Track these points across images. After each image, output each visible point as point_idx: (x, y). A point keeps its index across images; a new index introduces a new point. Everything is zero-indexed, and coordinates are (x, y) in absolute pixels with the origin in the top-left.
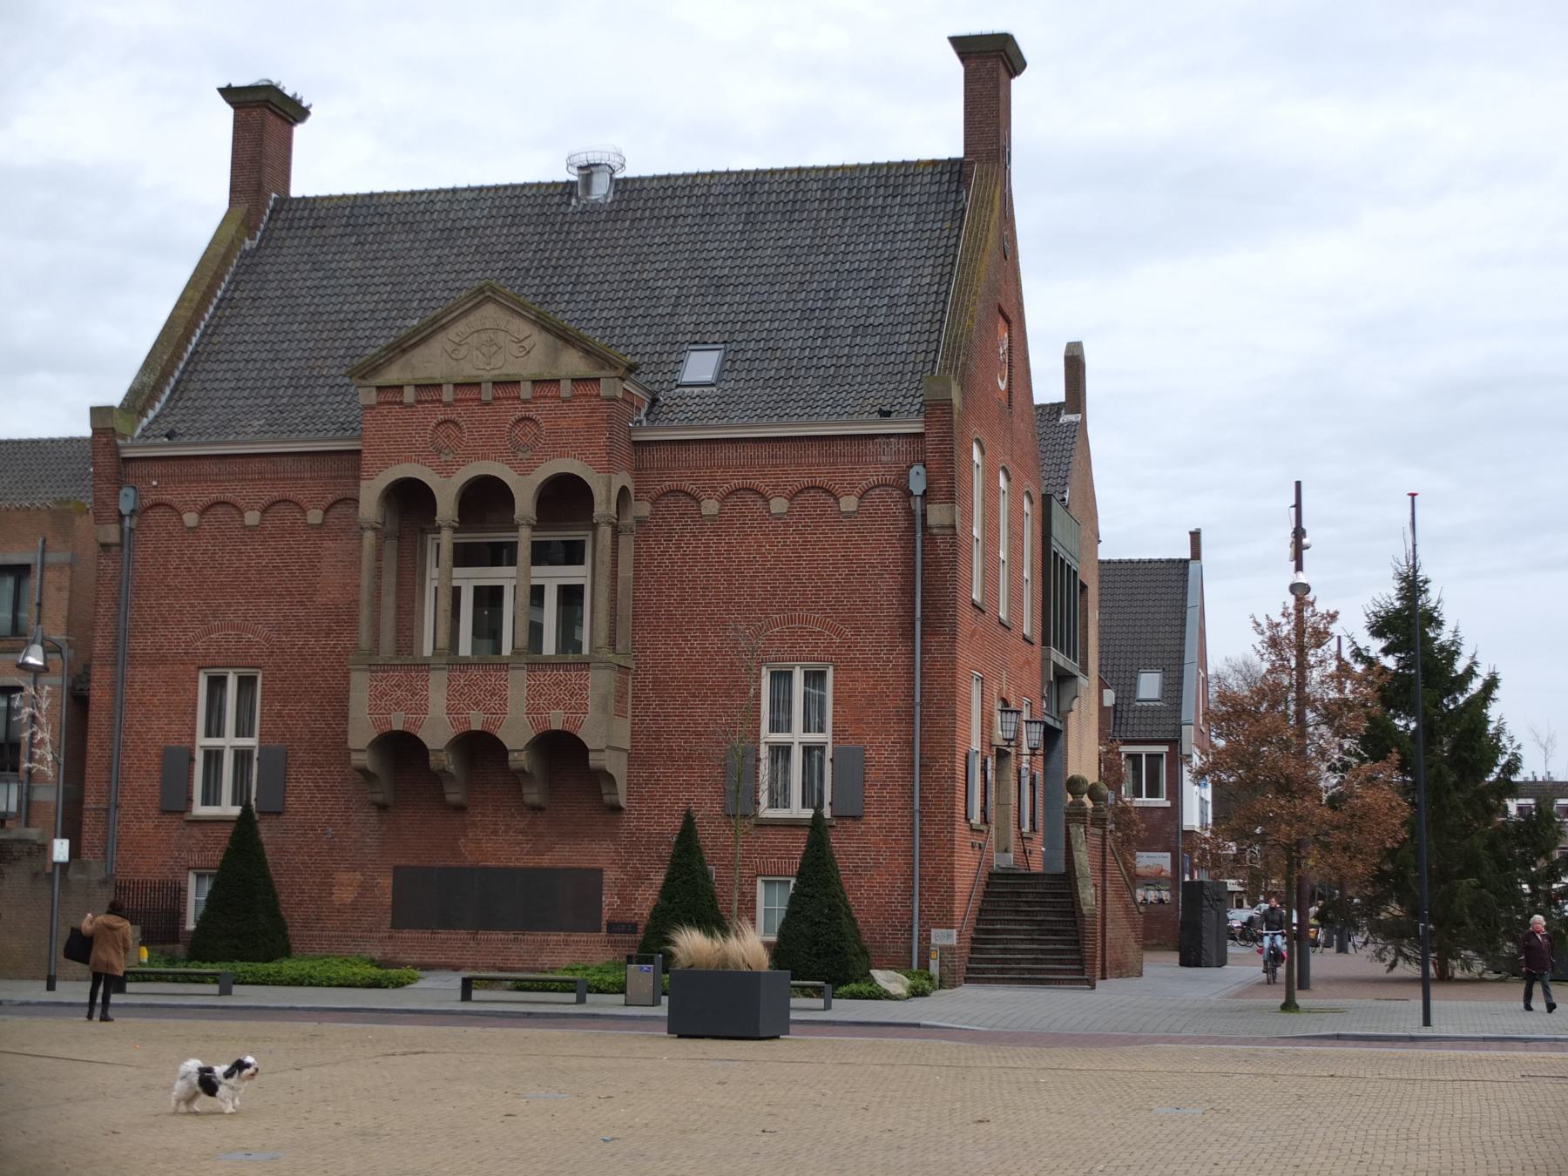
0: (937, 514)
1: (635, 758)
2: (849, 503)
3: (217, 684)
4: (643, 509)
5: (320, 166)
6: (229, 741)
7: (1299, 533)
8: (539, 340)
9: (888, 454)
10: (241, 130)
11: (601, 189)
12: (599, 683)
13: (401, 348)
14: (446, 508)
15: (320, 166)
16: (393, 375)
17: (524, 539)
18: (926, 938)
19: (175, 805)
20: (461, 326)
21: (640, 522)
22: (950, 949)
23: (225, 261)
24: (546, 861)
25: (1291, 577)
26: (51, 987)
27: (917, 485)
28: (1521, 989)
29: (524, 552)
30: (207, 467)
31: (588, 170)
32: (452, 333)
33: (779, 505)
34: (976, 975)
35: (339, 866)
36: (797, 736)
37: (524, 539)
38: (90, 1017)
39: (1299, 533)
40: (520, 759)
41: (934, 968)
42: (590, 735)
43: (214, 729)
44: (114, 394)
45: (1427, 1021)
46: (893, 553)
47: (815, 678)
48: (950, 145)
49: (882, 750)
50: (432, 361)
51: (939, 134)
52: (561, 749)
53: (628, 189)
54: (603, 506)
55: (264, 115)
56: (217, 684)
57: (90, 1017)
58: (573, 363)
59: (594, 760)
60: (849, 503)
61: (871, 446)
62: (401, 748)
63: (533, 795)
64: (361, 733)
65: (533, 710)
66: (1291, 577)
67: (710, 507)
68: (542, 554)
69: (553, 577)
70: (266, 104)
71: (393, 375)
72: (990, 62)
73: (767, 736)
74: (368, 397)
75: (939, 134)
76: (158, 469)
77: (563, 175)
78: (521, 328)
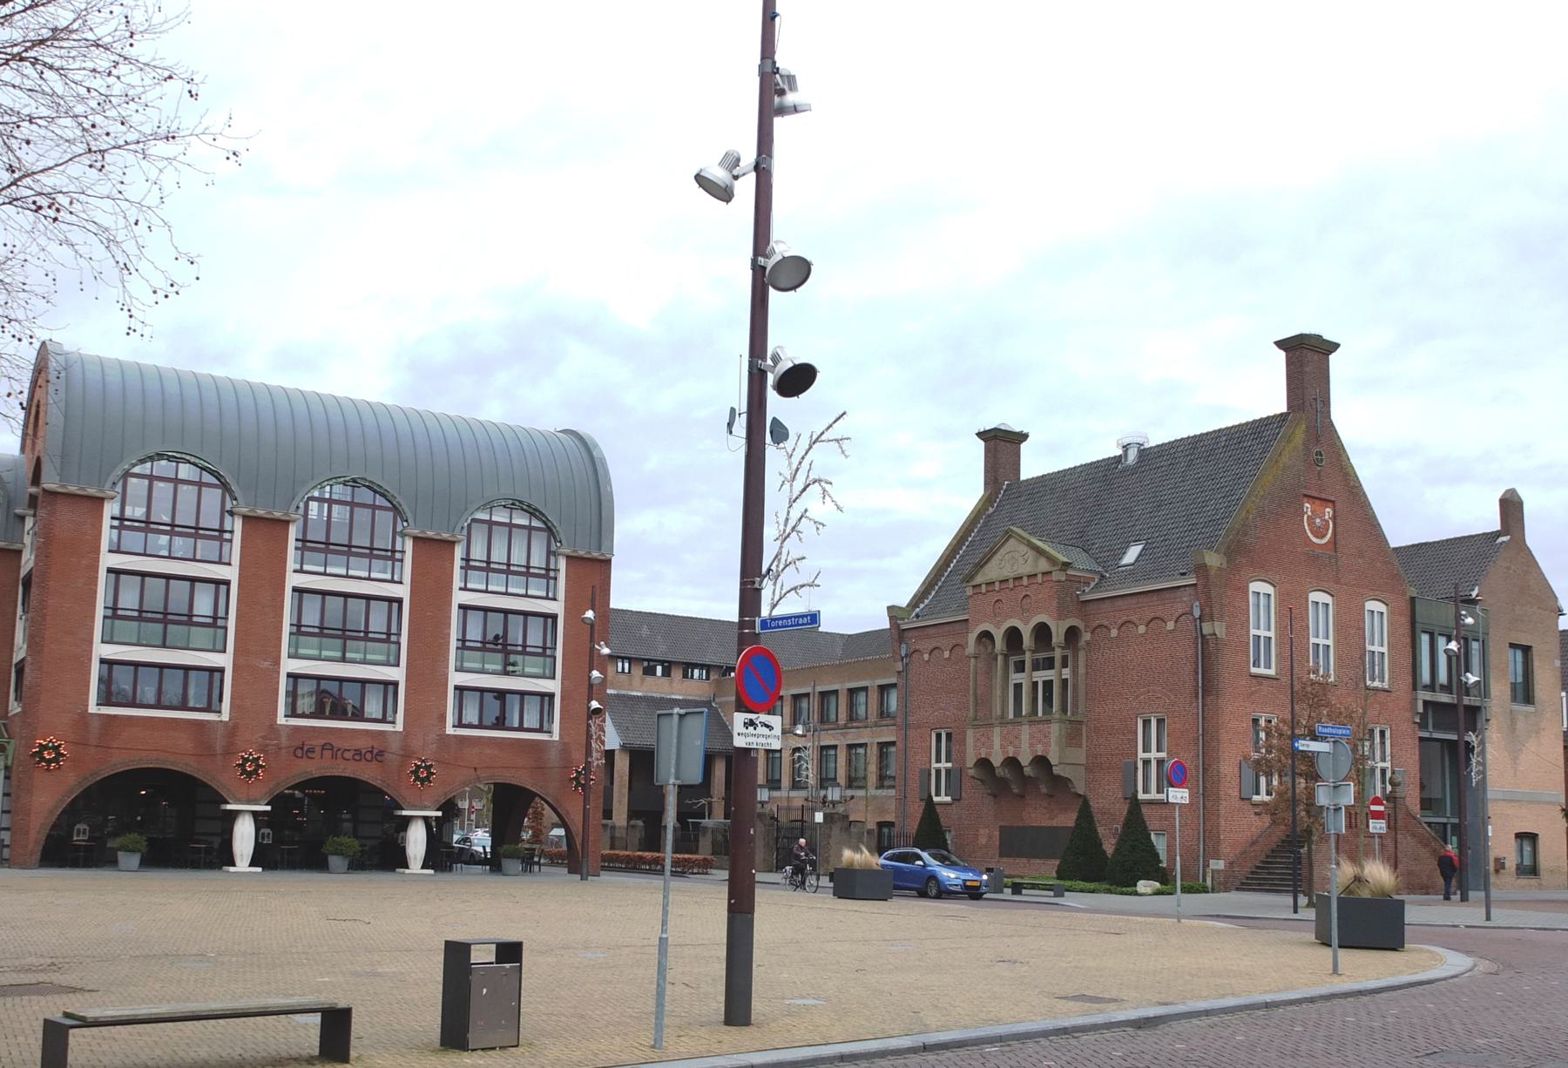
1: (1089, 769)
2: (1170, 625)
3: (939, 736)
5: (1033, 464)
8: (1031, 554)
9: (1186, 596)
10: (988, 452)
11: (1132, 455)
13: (980, 566)
15: (1033, 464)
17: (1058, 654)
18: (1206, 865)
20: (1002, 551)
21: (1088, 643)
22: (1218, 871)
24: (1054, 823)
27: (1197, 613)
28: (1289, 900)
29: (1028, 665)
30: (931, 631)
31: (1126, 448)
32: (998, 556)
33: (1142, 629)
34: (1243, 887)
35: (981, 823)
36: (944, 765)
37: (1028, 657)
38: (1447, 898)
40: (1028, 771)
41: (1209, 883)
43: (1146, 749)
44: (903, 600)
45: (1488, 918)
46: (1191, 652)
48: (1495, 524)
50: (993, 571)
51: (1266, 395)
52: (1041, 762)
53: (1145, 454)
54: (1058, 637)
55: (1002, 445)
56: (939, 736)
57: (1447, 898)
58: (1044, 565)
59: (1056, 770)
60: (1170, 625)
61: (1179, 593)
62: (984, 764)
63: (1044, 790)
64: (970, 762)
65: (1031, 745)
67: (1114, 633)
69: (1041, 676)
70: (995, 437)
71: (979, 579)
72: (1307, 357)
73: (1141, 755)
74: (969, 591)
75: (1266, 395)
76: (915, 633)
77: (1119, 452)
78: (1024, 549)
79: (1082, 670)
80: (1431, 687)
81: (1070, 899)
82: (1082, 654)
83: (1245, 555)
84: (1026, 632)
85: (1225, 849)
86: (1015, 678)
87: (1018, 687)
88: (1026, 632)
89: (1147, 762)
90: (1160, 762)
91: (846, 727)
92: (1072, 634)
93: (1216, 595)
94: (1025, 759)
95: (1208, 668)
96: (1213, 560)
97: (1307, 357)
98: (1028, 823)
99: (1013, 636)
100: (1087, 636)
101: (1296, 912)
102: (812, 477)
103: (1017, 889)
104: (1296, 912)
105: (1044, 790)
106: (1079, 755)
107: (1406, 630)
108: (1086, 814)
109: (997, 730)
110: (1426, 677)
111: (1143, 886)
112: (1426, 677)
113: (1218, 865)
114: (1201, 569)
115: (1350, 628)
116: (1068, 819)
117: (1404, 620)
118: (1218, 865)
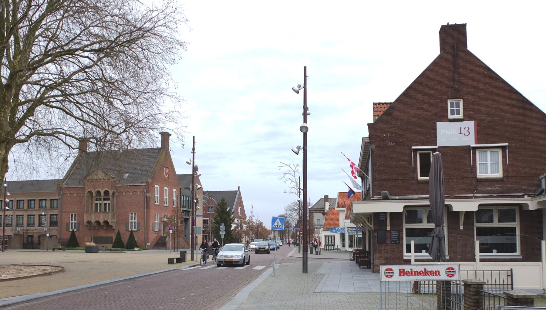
0: (147, 195)
1: (116, 224)
2: (138, 193)
3: (72, 215)
4: (117, 194)
6: (133, 221)
7: (305, 108)
12: (110, 215)
14: (102, 194)
16: (88, 178)
17: (102, 197)
19: (68, 230)
23: (74, 166)
25: (301, 123)
26: (417, 284)
29: (102, 199)
34: (153, 248)
36: (74, 222)
37: (102, 197)
39: (305, 108)
40: (102, 224)
42: (109, 221)
47: (135, 214)
49: (142, 222)
52: (106, 222)
54: (111, 194)
56: (72, 215)
60: (138, 193)
62: (89, 222)
63: (105, 228)
64: (85, 221)
66: (301, 123)
67: (124, 194)
68: (104, 199)
71: (88, 178)
73: (130, 221)
79: (115, 201)
80: (183, 207)
81: (66, 251)
82: (115, 198)
83: (155, 180)
84: (102, 192)
85: (150, 241)
86: (96, 202)
87: (97, 204)
88: (102, 192)
89: (132, 223)
90: (135, 222)
91: (27, 210)
92: (113, 194)
93: (149, 187)
94: (101, 221)
95: (147, 203)
96: (150, 181)
97: (239, 187)
98: (99, 236)
99: (99, 193)
100: (117, 194)
101: (512, 269)
102: (26, 144)
103: (54, 250)
104: (512, 269)
105: (105, 228)
106: (115, 221)
107: (179, 195)
108: (119, 233)
109: (93, 214)
110: (182, 205)
111: (136, 249)
112: (182, 205)
113: (149, 244)
114: (147, 182)
115: (171, 194)
116: (114, 236)
117: (179, 193)
118: (149, 244)
